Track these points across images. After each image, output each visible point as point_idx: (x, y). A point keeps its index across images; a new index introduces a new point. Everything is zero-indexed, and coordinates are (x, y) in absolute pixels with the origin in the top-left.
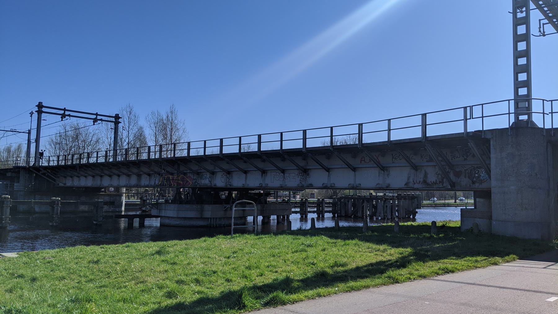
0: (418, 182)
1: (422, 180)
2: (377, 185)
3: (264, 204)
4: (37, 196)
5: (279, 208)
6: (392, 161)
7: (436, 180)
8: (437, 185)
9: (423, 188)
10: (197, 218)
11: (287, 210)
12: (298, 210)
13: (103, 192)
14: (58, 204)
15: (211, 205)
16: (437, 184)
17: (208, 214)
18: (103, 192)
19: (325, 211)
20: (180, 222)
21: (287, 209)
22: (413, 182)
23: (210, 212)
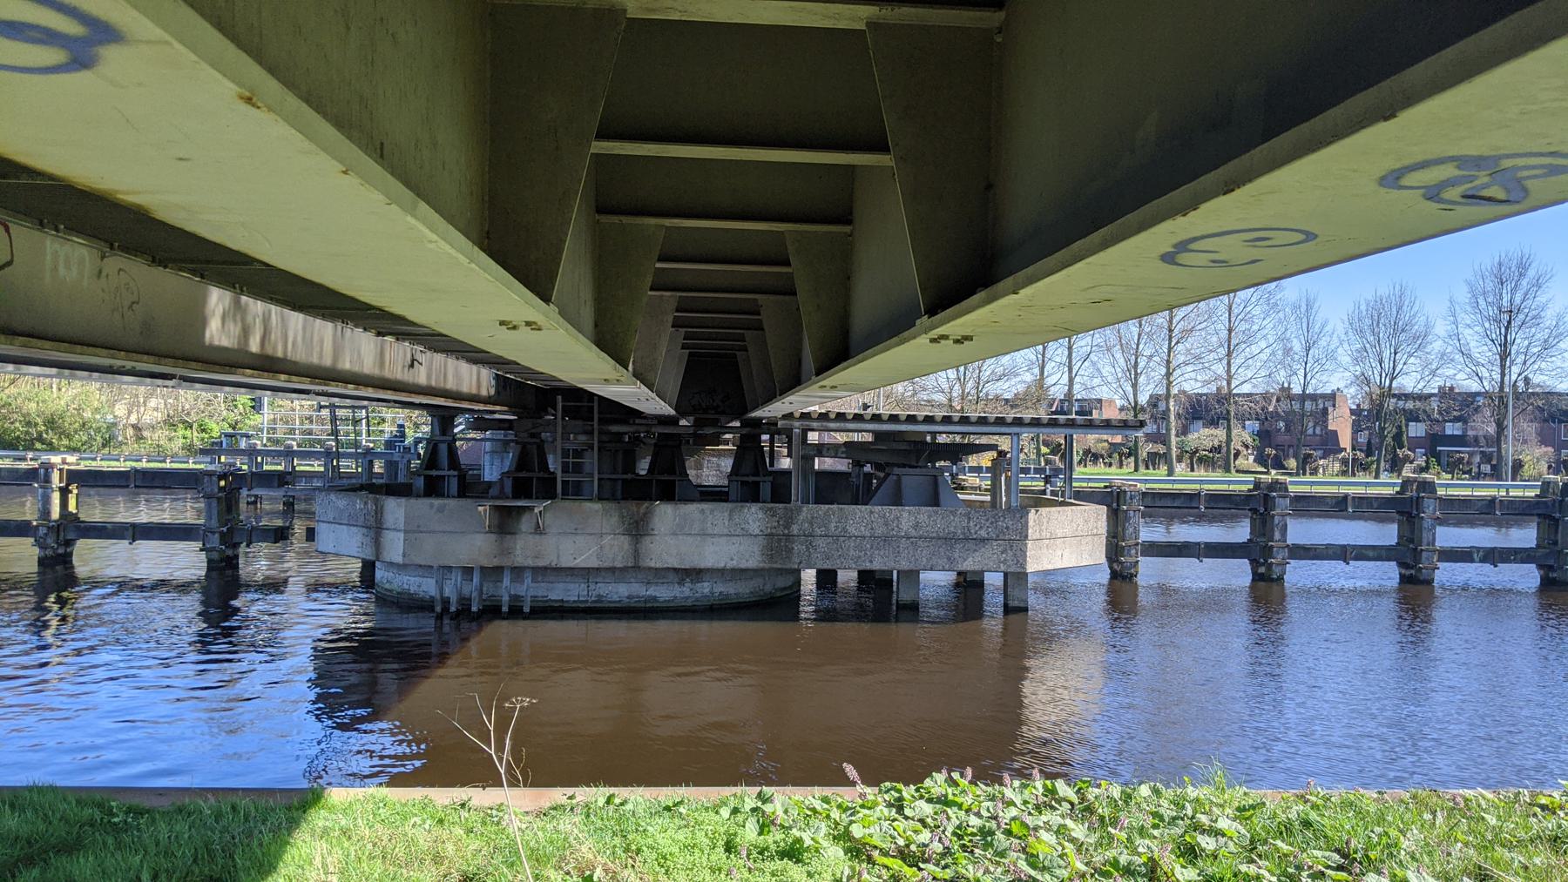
5: (916, 526)
14: (47, 480)
21: (983, 533)
23: (402, 535)
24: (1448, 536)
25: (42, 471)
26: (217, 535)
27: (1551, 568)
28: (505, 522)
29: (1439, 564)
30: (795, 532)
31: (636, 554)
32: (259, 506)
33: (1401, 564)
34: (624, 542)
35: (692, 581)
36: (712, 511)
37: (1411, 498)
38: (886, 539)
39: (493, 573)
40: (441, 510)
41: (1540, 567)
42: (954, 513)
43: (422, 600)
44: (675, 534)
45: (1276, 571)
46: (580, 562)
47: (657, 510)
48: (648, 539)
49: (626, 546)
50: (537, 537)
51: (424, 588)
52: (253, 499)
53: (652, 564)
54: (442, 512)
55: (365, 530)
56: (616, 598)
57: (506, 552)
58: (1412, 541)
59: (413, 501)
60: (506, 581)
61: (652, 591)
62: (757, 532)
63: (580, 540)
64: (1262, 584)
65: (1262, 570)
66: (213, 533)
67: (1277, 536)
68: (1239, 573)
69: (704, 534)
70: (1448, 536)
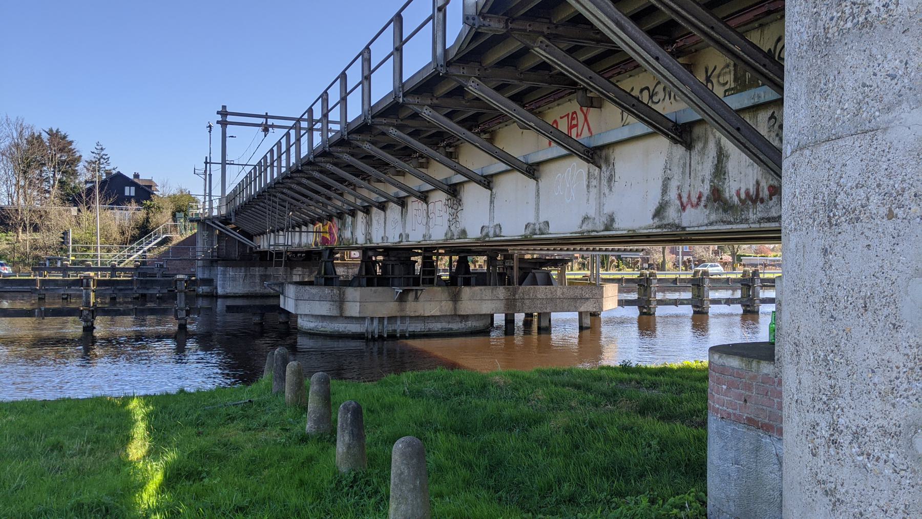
0: (694, 200)
1: (706, 189)
2: (583, 222)
3: (516, 286)
4: (219, 268)
5: (563, 294)
6: (622, 119)
7: (758, 183)
8: (760, 207)
9: (711, 224)
10: (330, 317)
11: (587, 299)
12: (688, 295)
13: (337, 259)
14: (88, 285)
15: (359, 288)
16: (762, 201)
17: (353, 309)
18: (337, 259)
19: (760, 300)
20: (316, 324)
21: (587, 296)
22: (678, 202)
23: (358, 304)
24: (713, 295)
25: (85, 281)
26: (184, 311)
27: (748, 306)
28: (402, 298)
29: (710, 306)
30: (517, 298)
31: (455, 309)
32: (69, 300)
33: (694, 306)
34: (450, 304)
35: (465, 322)
36: (485, 289)
37: (700, 278)
38: (551, 299)
39: (392, 319)
40: (375, 292)
41: (743, 305)
42: (576, 288)
43: (347, 334)
44: (470, 300)
45: (652, 310)
46: (433, 313)
47: (463, 291)
48: (460, 302)
49: (451, 306)
50: (415, 303)
51: (347, 329)
52: (66, 296)
53: (462, 313)
54: (376, 293)
55: (332, 303)
56: (436, 329)
57: (402, 310)
58: (699, 296)
59: (363, 288)
60: (399, 322)
61: (450, 326)
62: (502, 298)
63: (433, 303)
64: (645, 316)
65: (645, 310)
66: (182, 310)
67: (653, 296)
68: (688, 310)
69: (481, 300)
70: (713, 295)
